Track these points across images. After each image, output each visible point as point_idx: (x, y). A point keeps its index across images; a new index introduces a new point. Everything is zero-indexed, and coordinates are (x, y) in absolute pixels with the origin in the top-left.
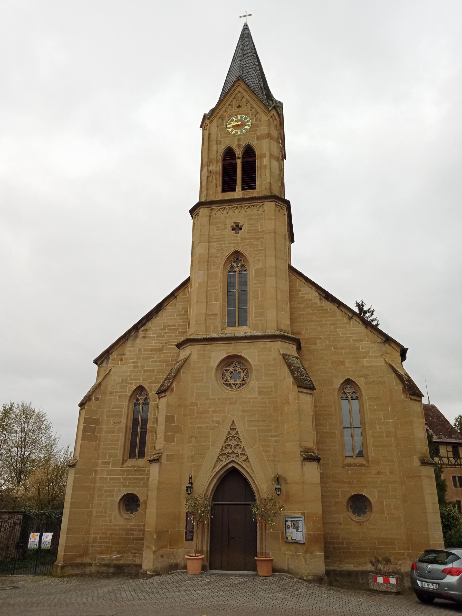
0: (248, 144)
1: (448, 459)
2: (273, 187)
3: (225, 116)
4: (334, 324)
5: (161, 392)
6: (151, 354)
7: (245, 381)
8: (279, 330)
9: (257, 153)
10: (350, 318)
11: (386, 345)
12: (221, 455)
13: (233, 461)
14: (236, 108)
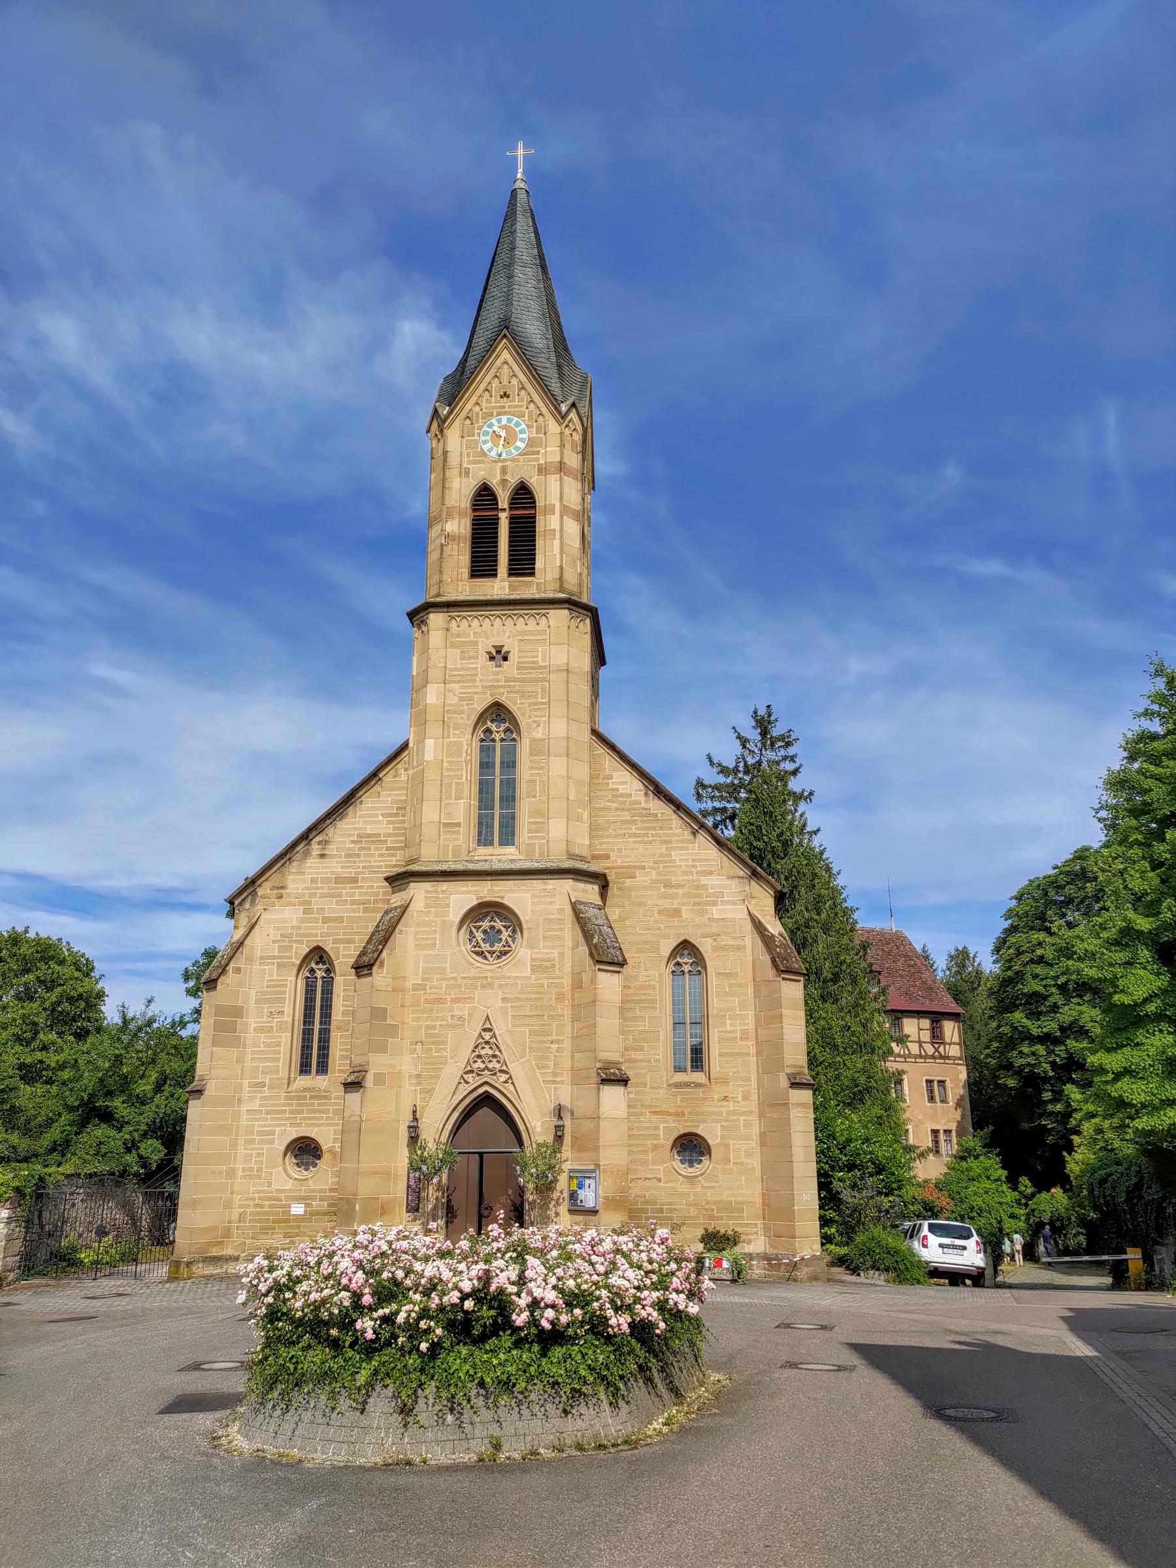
0: (522, 482)
1: (921, 1046)
2: (565, 576)
3: (478, 413)
4: (666, 842)
5: (363, 968)
6: (336, 889)
7: (509, 946)
8: (571, 856)
9: (540, 503)
10: (694, 833)
11: (752, 882)
12: (466, 1073)
13: (486, 1083)
14: (498, 397)
